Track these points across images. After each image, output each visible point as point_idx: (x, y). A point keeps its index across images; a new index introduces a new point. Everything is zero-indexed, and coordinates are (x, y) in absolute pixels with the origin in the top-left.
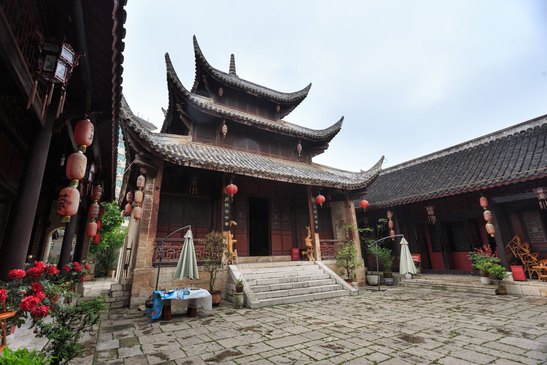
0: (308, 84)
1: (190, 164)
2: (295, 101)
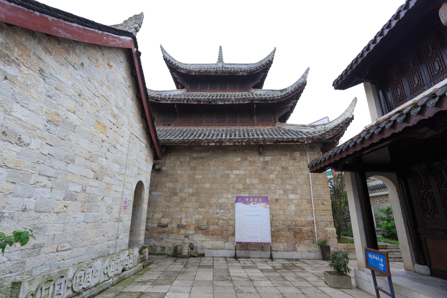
0: (273, 49)
1: (239, 101)
2: (263, 69)
